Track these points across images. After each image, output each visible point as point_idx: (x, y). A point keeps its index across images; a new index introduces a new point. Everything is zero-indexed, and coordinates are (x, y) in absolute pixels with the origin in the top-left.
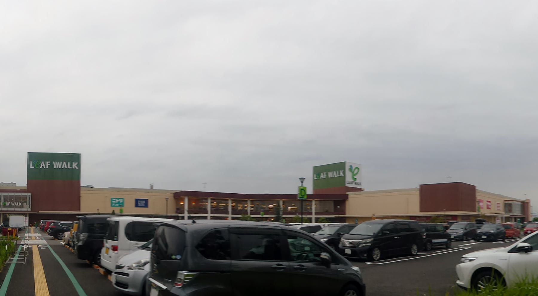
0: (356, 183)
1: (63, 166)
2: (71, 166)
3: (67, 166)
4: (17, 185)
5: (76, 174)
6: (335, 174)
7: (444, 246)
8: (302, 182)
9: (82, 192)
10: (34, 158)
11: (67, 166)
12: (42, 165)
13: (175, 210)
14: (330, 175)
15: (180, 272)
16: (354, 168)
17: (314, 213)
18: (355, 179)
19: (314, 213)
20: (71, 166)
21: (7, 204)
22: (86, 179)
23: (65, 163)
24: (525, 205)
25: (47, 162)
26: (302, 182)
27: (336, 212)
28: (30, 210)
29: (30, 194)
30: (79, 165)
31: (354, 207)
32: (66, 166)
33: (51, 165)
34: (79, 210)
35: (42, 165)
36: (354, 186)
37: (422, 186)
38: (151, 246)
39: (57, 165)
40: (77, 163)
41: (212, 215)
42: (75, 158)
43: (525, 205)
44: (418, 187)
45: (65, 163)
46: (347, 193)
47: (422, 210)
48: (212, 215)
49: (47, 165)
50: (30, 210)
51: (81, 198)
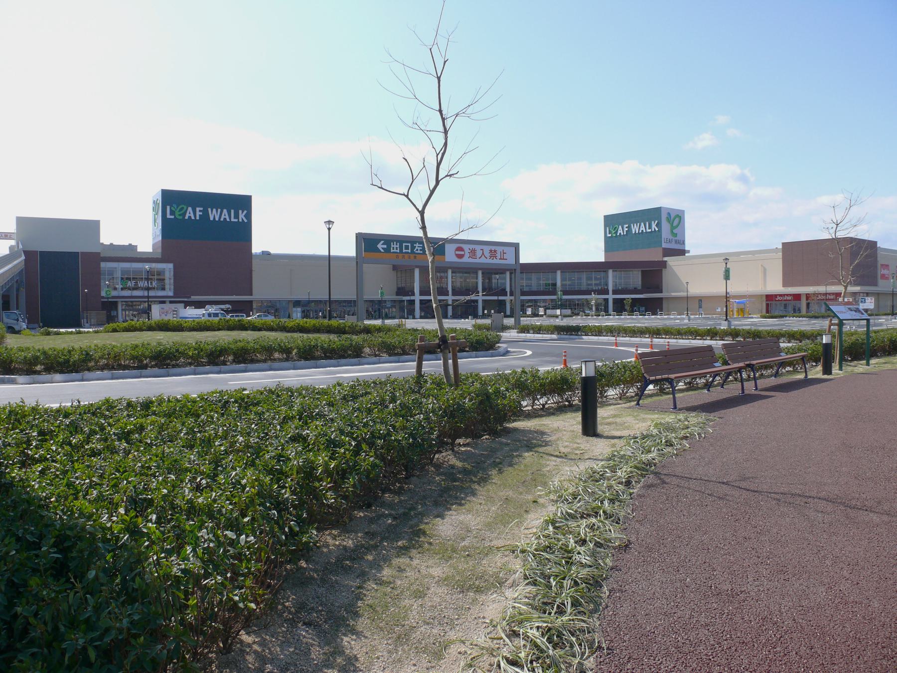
1: (223, 217)
2: (237, 216)
4: (139, 250)
5: (244, 231)
8: (329, 229)
9: (254, 261)
10: (172, 200)
12: (190, 213)
14: (635, 229)
15: (103, 294)
16: (673, 216)
17: (611, 292)
19: (611, 292)
20: (650, 227)
21: (130, 284)
22: (265, 238)
23: (225, 211)
25: (198, 209)
26: (329, 229)
27: (646, 288)
28: (171, 294)
29: (171, 266)
30: (249, 216)
31: (690, 278)
32: (227, 217)
33: (205, 215)
35: (190, 213)
36: (673, 246)
37: (788, 248)
38: (576, 401)
41: (473, 297)
42: (243, 203)
44: (780, 247)
45: (225, 211)
46: (665, 259)
47: (785, 284)
48: (473, 297)
49: (198, 213)
50: (171, 294)
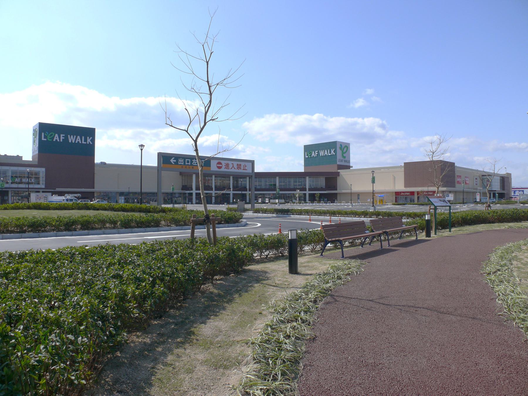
0: (345, 161)
2: (86, 140)
3: (82, 141)
4: (23, 159)
6: (326, 153)
7: (271, 253)
8: (142, 150)
9: (96, 168)
11: (82, 141)
13: (181, 187)
14: (322, 153)
17: (307, 190)
18: (345, 157)
19: (307, 190)
24: (505, 180)
25: (62, 135)
26: (142, 150)
27: (328, 187)
28: (43, 187)
30: (93, 140)
31: (352, 182)
33: (66, 139)
34: (94, 188)
39: (72, 139)
40: (91, 138)
43: (505, 180)
44: (403, 165)
45: (79, 137)
47: (406, 186)
49: (62, 138)
50: (43, 187)
51: (95, 175)
